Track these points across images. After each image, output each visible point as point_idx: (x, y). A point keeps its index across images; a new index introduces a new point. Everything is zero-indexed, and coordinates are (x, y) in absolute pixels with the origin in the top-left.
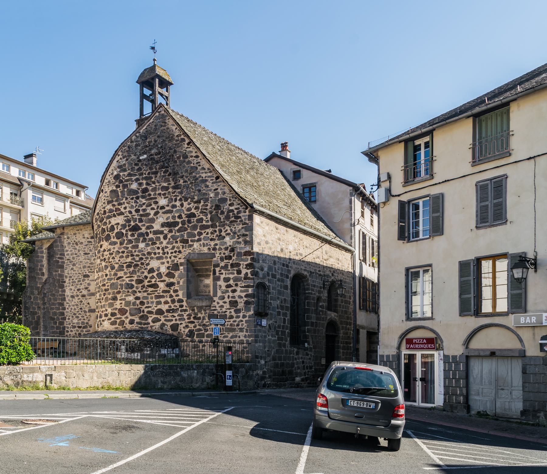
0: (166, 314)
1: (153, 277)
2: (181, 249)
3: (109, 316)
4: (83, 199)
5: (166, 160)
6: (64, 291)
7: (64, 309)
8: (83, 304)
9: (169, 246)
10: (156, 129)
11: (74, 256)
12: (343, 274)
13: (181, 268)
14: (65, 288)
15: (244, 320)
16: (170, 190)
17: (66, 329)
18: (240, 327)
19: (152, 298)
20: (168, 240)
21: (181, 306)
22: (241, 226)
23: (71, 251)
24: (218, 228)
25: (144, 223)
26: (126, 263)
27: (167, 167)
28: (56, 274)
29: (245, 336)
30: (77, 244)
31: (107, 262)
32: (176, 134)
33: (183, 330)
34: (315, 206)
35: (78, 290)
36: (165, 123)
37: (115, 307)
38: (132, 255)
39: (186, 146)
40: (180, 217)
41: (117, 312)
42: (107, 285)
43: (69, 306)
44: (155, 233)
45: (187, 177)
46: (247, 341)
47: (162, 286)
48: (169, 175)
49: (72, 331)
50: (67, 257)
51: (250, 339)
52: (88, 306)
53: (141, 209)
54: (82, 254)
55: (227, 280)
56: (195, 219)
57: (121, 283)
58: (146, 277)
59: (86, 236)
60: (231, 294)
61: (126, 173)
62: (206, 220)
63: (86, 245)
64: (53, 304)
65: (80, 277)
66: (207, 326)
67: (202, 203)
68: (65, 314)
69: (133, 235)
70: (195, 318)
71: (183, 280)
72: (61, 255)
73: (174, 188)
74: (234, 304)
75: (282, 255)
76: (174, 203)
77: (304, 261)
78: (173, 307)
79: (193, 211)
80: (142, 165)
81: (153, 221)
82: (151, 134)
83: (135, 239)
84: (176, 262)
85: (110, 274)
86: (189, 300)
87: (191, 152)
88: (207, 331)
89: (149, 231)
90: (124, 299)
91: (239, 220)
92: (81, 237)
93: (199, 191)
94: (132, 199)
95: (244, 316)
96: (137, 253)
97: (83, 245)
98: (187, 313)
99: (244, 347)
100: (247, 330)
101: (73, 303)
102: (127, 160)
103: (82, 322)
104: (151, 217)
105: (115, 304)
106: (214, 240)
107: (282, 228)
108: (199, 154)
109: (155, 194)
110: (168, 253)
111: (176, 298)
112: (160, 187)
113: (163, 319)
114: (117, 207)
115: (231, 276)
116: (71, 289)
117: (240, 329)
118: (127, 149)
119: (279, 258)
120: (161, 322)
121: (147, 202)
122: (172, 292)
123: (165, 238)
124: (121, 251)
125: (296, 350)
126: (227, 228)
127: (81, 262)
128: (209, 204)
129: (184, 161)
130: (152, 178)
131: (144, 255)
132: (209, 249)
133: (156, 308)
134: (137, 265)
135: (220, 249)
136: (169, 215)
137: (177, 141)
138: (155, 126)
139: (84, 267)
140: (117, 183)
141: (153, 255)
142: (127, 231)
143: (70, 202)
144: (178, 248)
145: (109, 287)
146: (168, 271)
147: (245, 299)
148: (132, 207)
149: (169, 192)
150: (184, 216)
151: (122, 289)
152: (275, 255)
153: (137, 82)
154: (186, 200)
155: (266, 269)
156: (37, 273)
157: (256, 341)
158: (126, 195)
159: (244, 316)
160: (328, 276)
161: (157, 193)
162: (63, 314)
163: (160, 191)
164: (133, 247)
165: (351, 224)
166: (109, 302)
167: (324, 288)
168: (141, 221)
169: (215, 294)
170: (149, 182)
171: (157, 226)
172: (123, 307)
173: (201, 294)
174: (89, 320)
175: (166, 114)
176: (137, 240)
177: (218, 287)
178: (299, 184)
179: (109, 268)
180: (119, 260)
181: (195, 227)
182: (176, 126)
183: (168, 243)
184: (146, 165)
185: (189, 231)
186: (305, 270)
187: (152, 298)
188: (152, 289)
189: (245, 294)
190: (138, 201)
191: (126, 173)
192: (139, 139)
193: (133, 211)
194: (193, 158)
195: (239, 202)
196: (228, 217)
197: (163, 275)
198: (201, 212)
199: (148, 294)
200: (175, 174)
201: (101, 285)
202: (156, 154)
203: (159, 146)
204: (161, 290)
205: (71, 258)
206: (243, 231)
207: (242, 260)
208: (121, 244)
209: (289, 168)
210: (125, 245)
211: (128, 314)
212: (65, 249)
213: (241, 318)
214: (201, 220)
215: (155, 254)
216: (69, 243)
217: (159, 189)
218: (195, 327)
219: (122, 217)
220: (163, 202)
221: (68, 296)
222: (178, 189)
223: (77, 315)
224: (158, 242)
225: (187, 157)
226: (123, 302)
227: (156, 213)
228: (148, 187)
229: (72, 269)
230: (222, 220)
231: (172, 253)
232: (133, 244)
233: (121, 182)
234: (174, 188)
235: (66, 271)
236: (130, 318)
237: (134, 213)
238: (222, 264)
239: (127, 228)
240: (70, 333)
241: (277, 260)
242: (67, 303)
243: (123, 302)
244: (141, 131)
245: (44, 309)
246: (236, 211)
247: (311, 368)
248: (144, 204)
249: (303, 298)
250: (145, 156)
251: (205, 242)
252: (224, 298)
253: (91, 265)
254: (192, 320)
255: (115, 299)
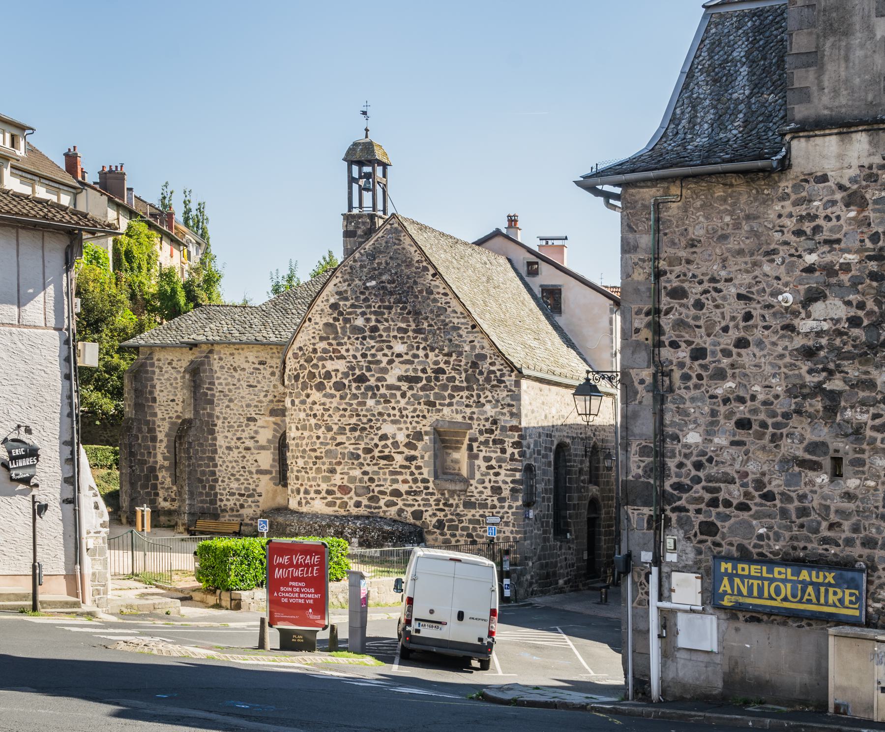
0: (405, 497)
1: (386, 446)
2: (426, 413)
3: (324, 494)
4: (23, 154)
5: (403, 292)
6: (215, 439)
7: (215, 466)
8: (248, 461)
9: (408, 407)
10: (387, 247)
11: (231, 387)
12: (605, 431)
13: (426, 438)
14: (216, 435)
15: (510, 511)
16: (410, 334)
17: (219, 497)
18: (505, 520)
19: (385, 474)
20: (407, 399)
21: (427, 488)
22: (505, 393)
23: (225, 379)
24: (476, 392)
25: (373, 373)
26: (350, 424)
27: (405, 303)
28: (204, 414)
29: (512, 532)
30: (235, 369)
31: (319, 420)
32: (416, 259)
33: (429, 519)
34: (561, 320)
35: (239, 439)
36: (400, 240)
37: (333, 482)
38: (358, 415)
39: (431, 278)
40: (424, 371)
41: (336, 489)
42: (319, 451)
43: (224, 462)
44: (390, 387)
45: (433, 320)
46: (514, 538)
47: (399, 459)
48: (407, 314)
49: (228, 500)
50: (220, 388)
51: (518, 536)
52: (256, 464)
53: (369, 353)
54: (245, 386)
55: (487, 459)
56: (445, 376)
57: (343, 451)
58: (376, 446)
59: (251, 359)
60: (493, 478)
61: (348, 303)
62: (460, 379)
63: (252, 373)
64: (202, 459)
65: (242, 420)
66: (462, 516)
67: (454, 356)
68: (217, 473)
69: (358, 388)
70: (445, 504)
71: (428, 453)
72: (210, 383)
73: (414, 331)
74: (496, 490)
75: (545, 424)
76: (415, 351)
77: (566, 425)
78: (414, 489)
79: (442, 365)
80: (370, 294)
81: (385, 371)
82: (380, 252)
83: (362, 394)
84: (418, 429)
85: (325, 438)
86: (437, 482)
87: (438, 287)
88: (462, 522)
89: (380, 384)
90: (347, 474)
91: (502, 385)
92: (243, 360)
93: (450, 340)
94: (357, 339)
95: (510, 507)
96: (364, 413)
97: (246, 373)
98: (435, 497)
99: (510, 546)
100: (514, 524)
101: (230, 458)
102: (349, 285)
103: (246, 488)
104: (382, 365)
105: (333, 478)
106: (471, 406)
107: (545, 387)
108: (447, 291)
109: (388, 336)
110: (407, 417)
111: (420, 477)
112: (396, 328)
113: (400, 503)
114: (335, 347)
115: (493, 455)
116: (227, 437)
117: (505, 522)
118: (349, 271)
119: (543, 428)
120: (398, 507)
121: (377, 345)
122: (413, 469)
123: (403, 395)
124: (341, 407)
125: (559, 543)
126: (488, 393)
127: (242, 397)
128: (463, 360)
129: (429, 298)
130: (384, 314)
131: (374, 415)
132: (464, 417)
133: (390, 488)
134: (364, 429)
135: (479, 419)
136: (408, 366)
137: (417, 268)
138: (386, 242)
139: (248, 406)
140: (335, 315)
141: (386, 417)
142: (350, 382)
143: (12, 167)
144: (421, 411)
145: (323, 455)
146: (407, 440)
147: (512, 485)
148: (357, 350)
149: (409, 336)
150: (429, 371)
151: (344, 459)
152: (540, 425)
153: (344, 159)
154: (433, 350)
155: (532, 446)
156: (146, 398)
157: (525, 539)
158: (348, 333)
159: (510, 507)
160: (589, 438)
161: (392, 334)
162: (213, 473)
163: (395, 333)
164: (359, 404)
165: (612, 354)
166: (323, 474)
167: (586, 456)
168: (369, 369)
169: (472, 475)
170: (379, 318)
171: (391, 379)
172: (345, 483)
173: (451, 471)
174: (257, 486)
175: (400, 228)
176: (364, 395)
177: (476, 468)
178: (536, 283)
179: (323, 429)
180: (339, 420)
181: (444, 387)
182: (415, 248)
183: (407, 403)
184: (375, 295)
185: (436, 390)
186: (568, 437)
187: (385, 474)
188: (385, 462)
189: (511, 478)
190: (365, 342)
191: (348, 303)
192: (364, 258)
193: (358, 355)
194: (440, 296)
195: (503, 362)
196: (488, 380)
197: (401, 446)
198: (453, 369)
199: (380, 468)
200: (417, 313)
201: (307, 449)
202: (390, 282)
203: (393, 271)
204: (399, 464)
205: (226, 390)
206: (508, 400)
207: (508, 436)
208: (342, 398)
209: (523, 257)
210: (347, 401)
211: (352, 493)
212: (215, 376)
213: (506, 509)
214: (452, 379)
215: (389, 415)
216: (222, 367)
217: (394, 329)
218: (446, 516)
219: (343, 362)
220: (399, 348)
221: (221, 447)
222: (421, 333)
223: (237, 476)
224: (393, 401)
225: (432, 293)
226: (346, 477)
227: (391, 362)
228: (379, 325)
229: (228, 406)
230: (481, 382)
231: (413, 417)
232: (360, 400)
233: (340, 313)
234: (414, 331)
235: (217, 409)
236: (356, 498)
237: (359, 358)
238: (482, 439)
239: (351, 378)
240: (225, 502)
241: (541, 431)
242: (221, 457)
243: (346, 477)
244: (367, 247)
245: (189, 466)
246: (498, 374)
247: (573, 565)
248: (373, 347)
249: (564, 472)
250: (374, 283)
251: (459, 408)
252: (484, 482)
253: (260, 405)
254: (441, 506)
255: (333, 471)
